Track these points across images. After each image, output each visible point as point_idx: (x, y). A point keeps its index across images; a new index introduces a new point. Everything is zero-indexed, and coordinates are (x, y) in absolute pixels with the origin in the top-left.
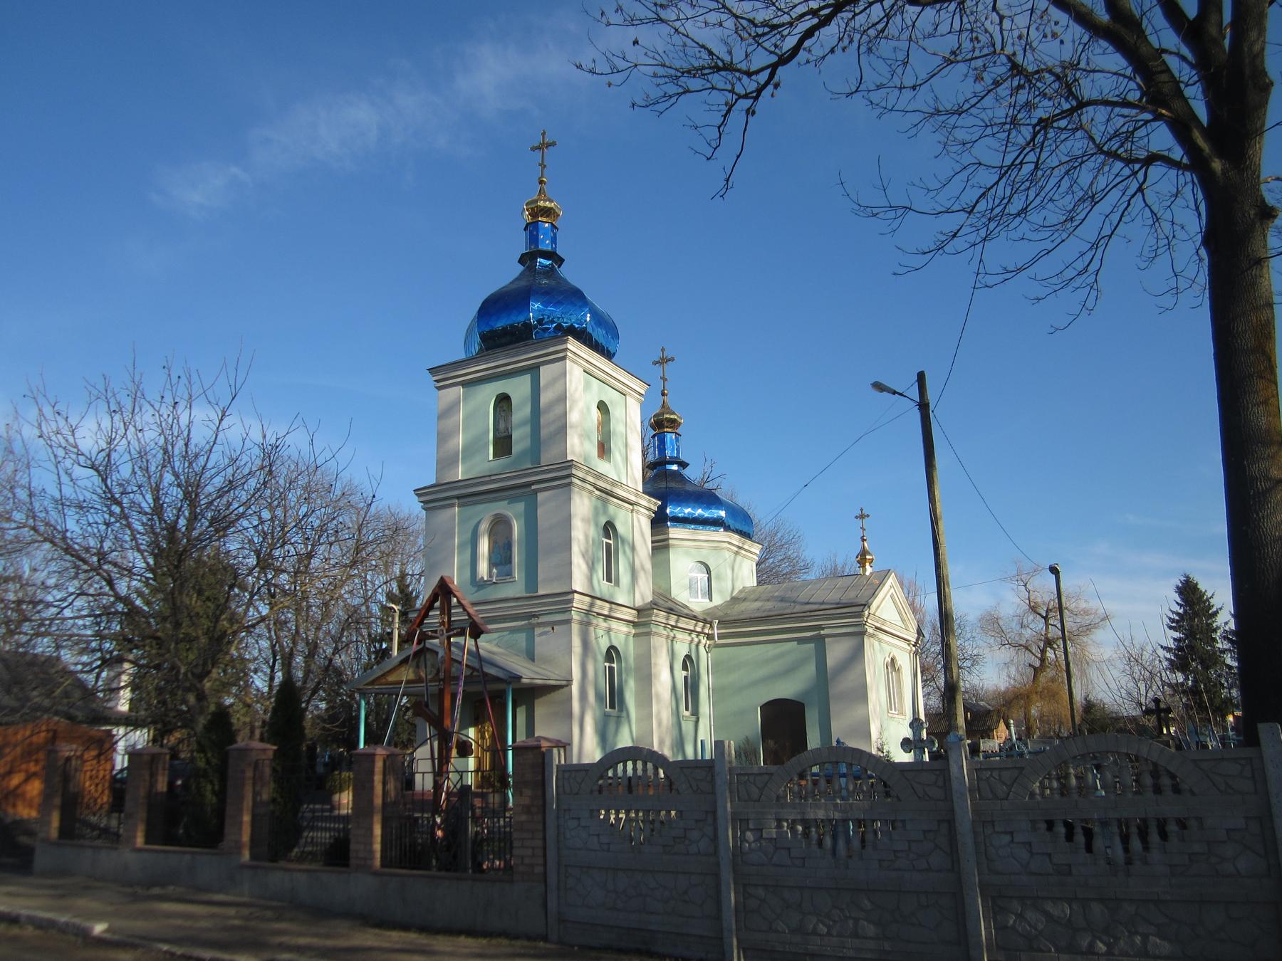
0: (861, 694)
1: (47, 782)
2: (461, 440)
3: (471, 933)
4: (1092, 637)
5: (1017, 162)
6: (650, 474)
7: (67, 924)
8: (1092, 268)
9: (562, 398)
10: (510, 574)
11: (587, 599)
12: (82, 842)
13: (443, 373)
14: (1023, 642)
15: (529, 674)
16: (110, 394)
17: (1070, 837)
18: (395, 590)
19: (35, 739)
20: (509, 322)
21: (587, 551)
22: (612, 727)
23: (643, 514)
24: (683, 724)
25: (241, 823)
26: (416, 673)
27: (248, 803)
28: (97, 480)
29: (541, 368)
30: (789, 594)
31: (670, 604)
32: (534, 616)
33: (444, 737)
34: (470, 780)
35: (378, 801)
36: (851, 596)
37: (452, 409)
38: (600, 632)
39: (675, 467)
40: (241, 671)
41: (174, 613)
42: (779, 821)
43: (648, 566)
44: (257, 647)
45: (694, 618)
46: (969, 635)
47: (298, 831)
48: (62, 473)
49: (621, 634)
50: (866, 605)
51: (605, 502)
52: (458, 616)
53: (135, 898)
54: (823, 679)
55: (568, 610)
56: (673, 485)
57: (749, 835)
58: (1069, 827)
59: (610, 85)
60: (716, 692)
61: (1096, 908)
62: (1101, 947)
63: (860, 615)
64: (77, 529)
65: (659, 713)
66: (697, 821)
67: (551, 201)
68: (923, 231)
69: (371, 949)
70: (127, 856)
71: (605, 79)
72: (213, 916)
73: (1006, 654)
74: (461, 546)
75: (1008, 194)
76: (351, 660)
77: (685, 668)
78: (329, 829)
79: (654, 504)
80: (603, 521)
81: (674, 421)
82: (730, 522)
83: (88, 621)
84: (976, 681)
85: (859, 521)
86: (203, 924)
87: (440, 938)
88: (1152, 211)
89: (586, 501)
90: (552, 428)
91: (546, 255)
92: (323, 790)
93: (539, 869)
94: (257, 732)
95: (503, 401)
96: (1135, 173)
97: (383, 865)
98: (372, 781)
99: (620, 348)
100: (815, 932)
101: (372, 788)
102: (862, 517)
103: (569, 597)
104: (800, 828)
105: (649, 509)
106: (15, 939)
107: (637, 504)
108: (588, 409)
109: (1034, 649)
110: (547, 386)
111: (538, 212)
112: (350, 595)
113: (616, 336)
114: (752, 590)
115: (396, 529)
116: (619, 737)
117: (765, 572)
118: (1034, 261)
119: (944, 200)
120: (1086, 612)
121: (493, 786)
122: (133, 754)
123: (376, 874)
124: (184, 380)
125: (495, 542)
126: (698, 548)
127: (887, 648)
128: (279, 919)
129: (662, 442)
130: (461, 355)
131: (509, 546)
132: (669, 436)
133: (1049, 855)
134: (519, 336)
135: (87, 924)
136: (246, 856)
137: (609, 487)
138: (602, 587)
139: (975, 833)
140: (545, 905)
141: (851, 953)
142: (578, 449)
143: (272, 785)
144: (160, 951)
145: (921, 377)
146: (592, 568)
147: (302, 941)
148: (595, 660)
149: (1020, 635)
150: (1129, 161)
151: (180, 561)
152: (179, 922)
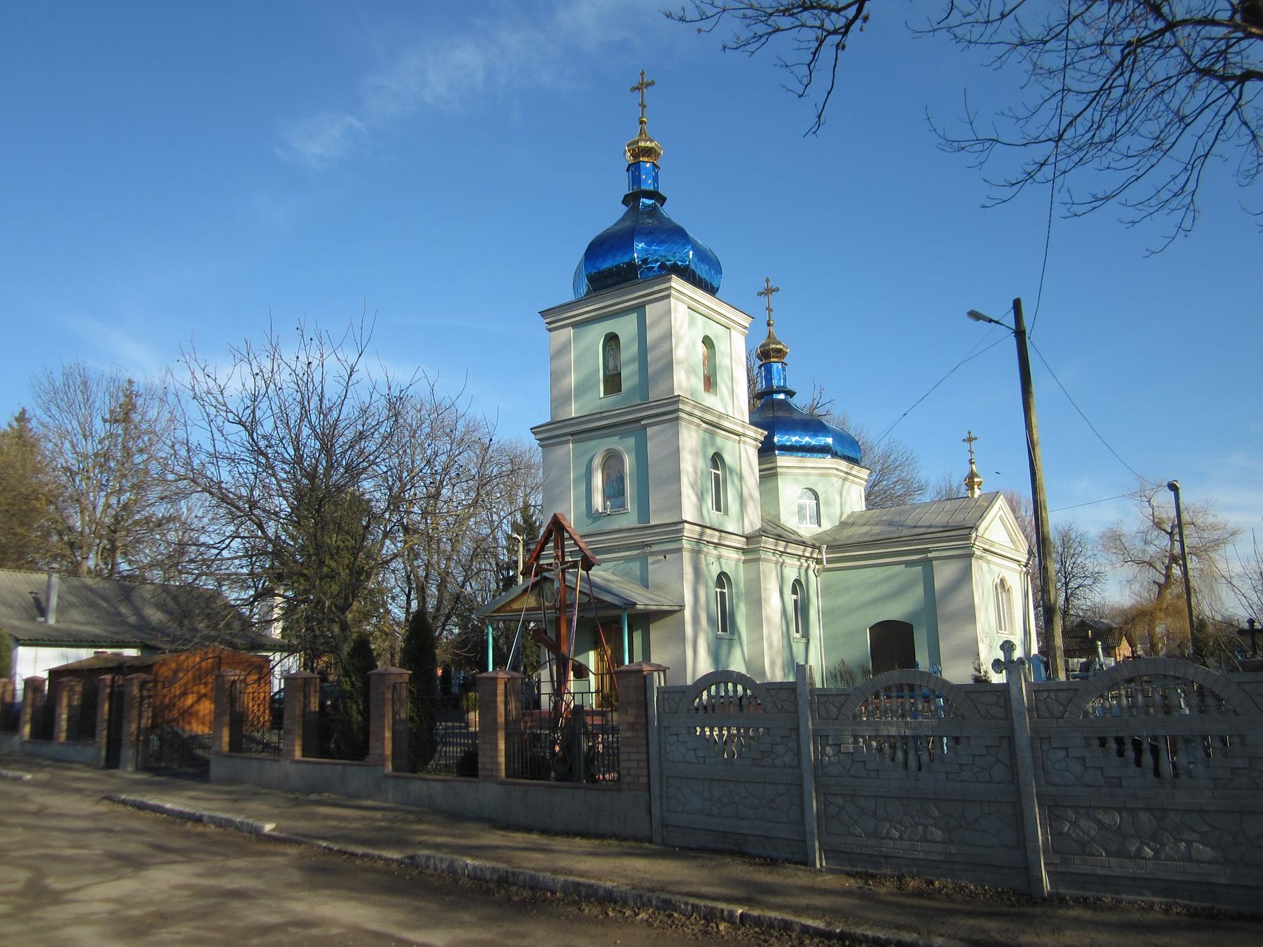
0: (969, 614)
1: (216, 701)
2: (573, 379)
3: (585, 835)
4: (1221, 552)
5: (1107, 86)
6: (759, 403)
7: (242, 823)
8: (1190, 187)
9: (668, 335)
10: (623, 506)
11: (698, 528)
12: (248, 754)
13: (553, 316)
14: (1147, 559)
15: (644, 600)
16: (252, 357)
17: (1120, 753)
18: (520, 520)
19: (203, 664)
20: (615, 263)
21: (696, 482)
22: (724, 649)
23: (750, 445)
24: (794, 645)
25: (384, 738)
27: (388, 721)
28: (245, 435)
30: (897, 518)
31: (779, 531)
32: (648, 545)
33: (562, 664)
34: (592, 701)
35: (501, 719)
36: (958, 519)
37: (563, 349)
38: (711, 559)
39: (782, 396)
40: (377, 605)
41: (317, 550)
42: (856, 737)
43: (756, 494)
44: (393, 580)
45: (803, 543)
46: (1090, 553)
47: (434, 745)
48: (215, 430)
49: (731, 561)
50: (974, 528)
51: (712, 434)
53: (297, 802)
54: (931, 600)
55: (679, 540)
56: (780, 414)
57: (829, 750)
58: (1120, 741)
59: (700, 31)
60: (826, 614)
61: (1144, 817)
62: (1149, 852)
63: (968, 537)
64: (229, 479)
65: (769, 636)
66: (782, 737)
67: (652, 141)
68: (1012, 162)
69: (498, 847)
70: (286, 767)
71: (697, 25)
72: (363, 818)
73: (1130, 570)
74: (576, 480)
75: (1097, 118)
76: (483, 588)
77: (794, 592)
78: (460, 744)
79: (761, 434)
80: (711, 452)
81: (780, 351)
82: (839, 449)
83: (244, 562)
84: (1097, 599)
85: (967, 444)
86: (355, 825)
87: (558, 839)
88: (1249, 127)
89: (694, 434)
90: (659, 365)
91: (653, 195)
92: (456, 709)
93: (644, 780)
94: (397, 657)
95: (612, 340)
96: (1230, 91)
97: (507, 776)
98: (496, 702)
99: (724, 283)
100: (888, 837)
101: (496, 708)
102: (970, 440)
103: (680, 527)
104: (874, 744)
105: (756, 440)
106: (201, 835)
107: (744, 435)
108: (694, 345)
110: (654, 323)
111: (640, 153)
112: (477, 526)
113: (719, 270)
114: (861, 514)
115: (517, 467)
116: (732, 659)
117: (871, 497)
118: (1124, 187)
119: (1032, 130)
120: (1214, 527)
121: (612, 705)
122: (288, 678)
123: (501, 783)
124: (316, 341)
125: (608, 476)
126: (807, 475)
127: (996, 569)
128: (419, 821)
129: (769, 372)
130: (571, 297)
132: (775, 366)
133: (1102, 769)
134: (625, 277)
135: (258, 824)
136: (389, 767)
137: (715, 420)
138: (712, 516)
139: (1033, 748)
140: (650, 812)
141: (921, 855)
142: (684, 383)
143: (409, 705)
144: (320, 846)
145: (1017, 305)
146: (701, 498)
147: (439, 840)
148: (707, 586)
149: (1144, 551)
150: (1223, 79)
151: (320, 506)
152: (334, 823)
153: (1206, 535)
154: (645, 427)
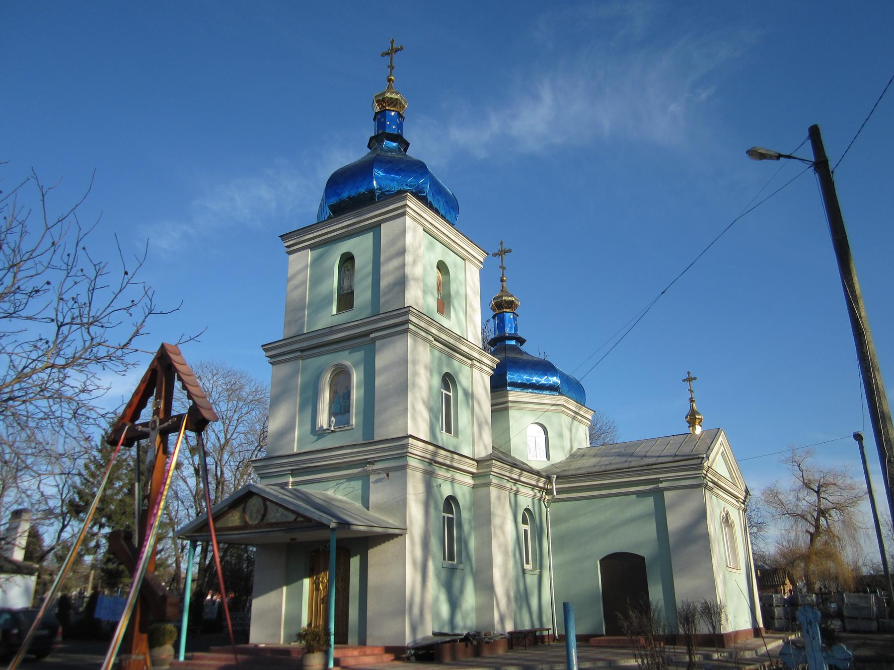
10: (348, 423)
11: (431, 448)
14: (800, 513)
23: (487, 373)
26: (243, 518)
29: (382, 226)
39: (513, 342)
45: (531, 471)
46: (754, 507)
49: (460, 486)
52: (180, 405)
55: (404, 456)
63: (700, 466)
67: (397, 93)
85: (687, 384)
95: (348, 259)
103: (404, 442)
109: (809, 518)
117: (594, 435)
131: (348, 395)
137: (452, 341)
145: (815, 134)
149: (797, 506)
153: (845, 494)
154: (374, 340)
